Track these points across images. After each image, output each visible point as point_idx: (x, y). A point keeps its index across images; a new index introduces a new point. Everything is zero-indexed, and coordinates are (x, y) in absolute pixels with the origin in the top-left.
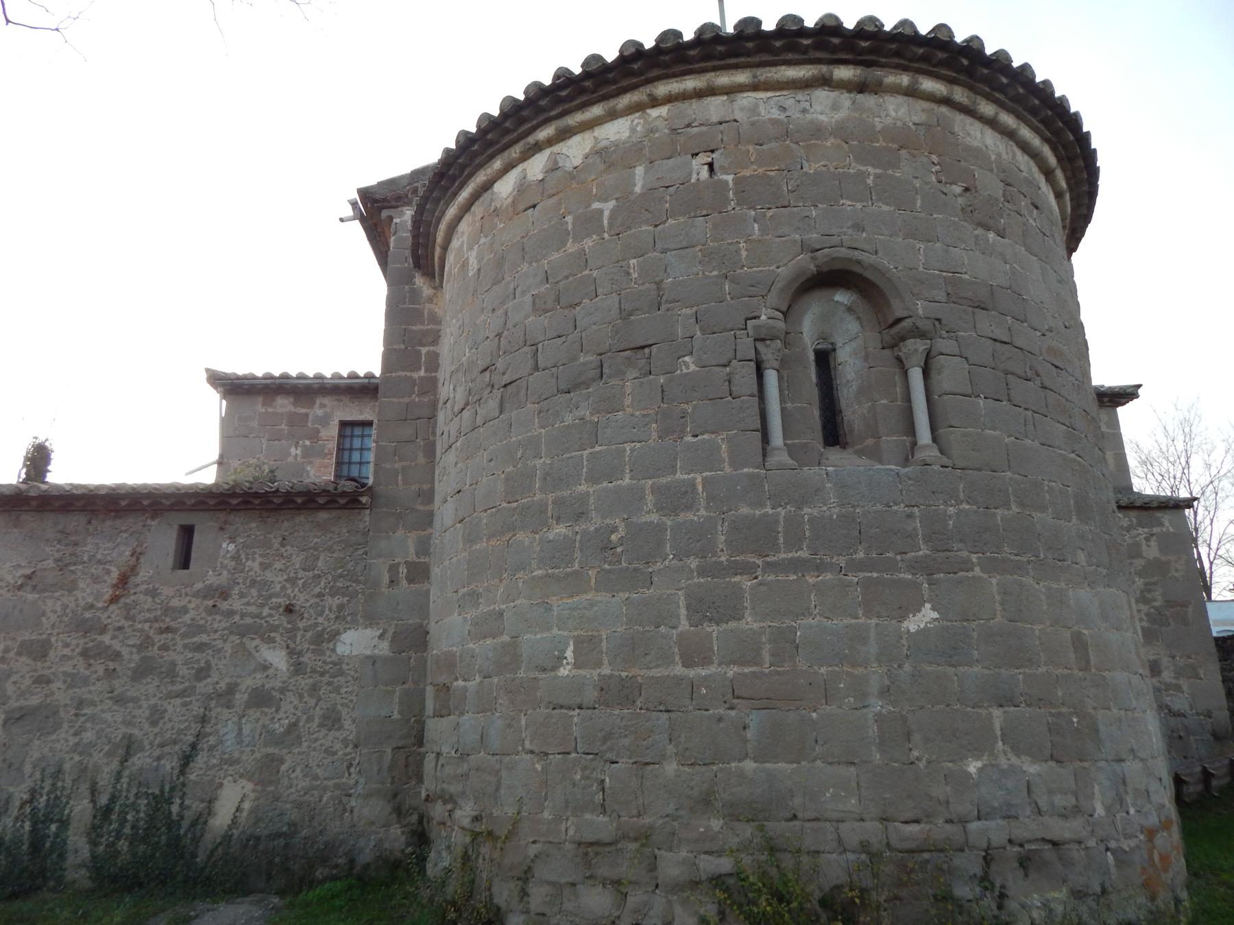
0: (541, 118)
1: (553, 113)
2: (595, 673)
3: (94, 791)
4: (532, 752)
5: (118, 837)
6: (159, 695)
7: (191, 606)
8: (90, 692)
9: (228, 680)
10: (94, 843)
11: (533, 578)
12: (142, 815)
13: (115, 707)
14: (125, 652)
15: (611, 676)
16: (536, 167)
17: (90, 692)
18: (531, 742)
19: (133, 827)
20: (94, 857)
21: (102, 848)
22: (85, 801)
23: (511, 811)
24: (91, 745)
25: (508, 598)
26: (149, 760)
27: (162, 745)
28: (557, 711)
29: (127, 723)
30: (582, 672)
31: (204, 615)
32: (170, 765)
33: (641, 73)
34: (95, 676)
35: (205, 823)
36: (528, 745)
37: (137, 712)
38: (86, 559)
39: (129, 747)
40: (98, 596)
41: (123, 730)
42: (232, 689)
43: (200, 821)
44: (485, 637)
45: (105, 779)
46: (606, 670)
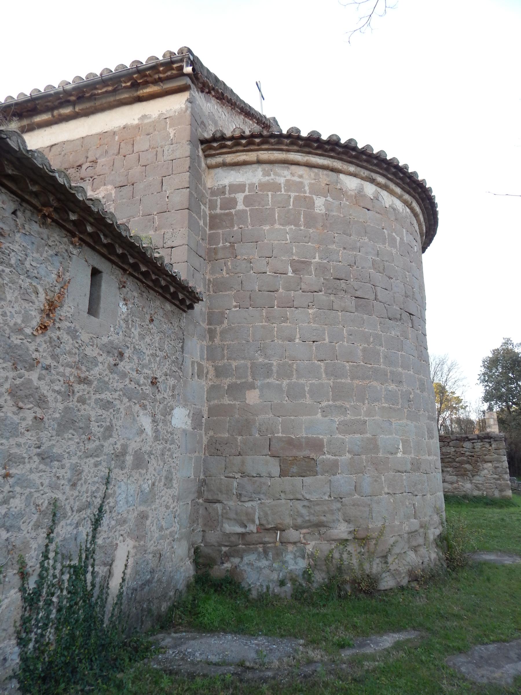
0: (385, 173)
1: (389, 176)
2: (410, 456)
3: (24, 575)
4: (388, 493)
5: (45, 626)
6: (79, 454)
7: (100, 359)
8: (18, 445)
9: (122, 441)
10: (22, 642)
11: (384, 407)
12: (65, 592)
13: (42, 467)
14: (51, 397)
15: (414, 458)
16: (370, 189)
17: (18, 445)
18: (388, 488)
19: (59, 610)
20: (24, 659)
21: (31, 646)
22: (13, 592)
23: (380, 525)
24: (21, 515)
25: (369, 413)
26: (70, 528)
27: (79, 511)
28: (397, 473)
29: (54, 487)
30: (406, 456)
31: (107, 372)
32: (86, 529)
33: (339, 153)
34: (24, 424)
35: (108, 588)
36: (386, 490)
37: (61, 473)
38: (13, 261)
39: (55, 513)
40: (27, 318)
41: (50, 494)
42: (124, 452)
43: (105, 587)
44: (354, 433)
45: (33, 560)
46: (413, 456)
